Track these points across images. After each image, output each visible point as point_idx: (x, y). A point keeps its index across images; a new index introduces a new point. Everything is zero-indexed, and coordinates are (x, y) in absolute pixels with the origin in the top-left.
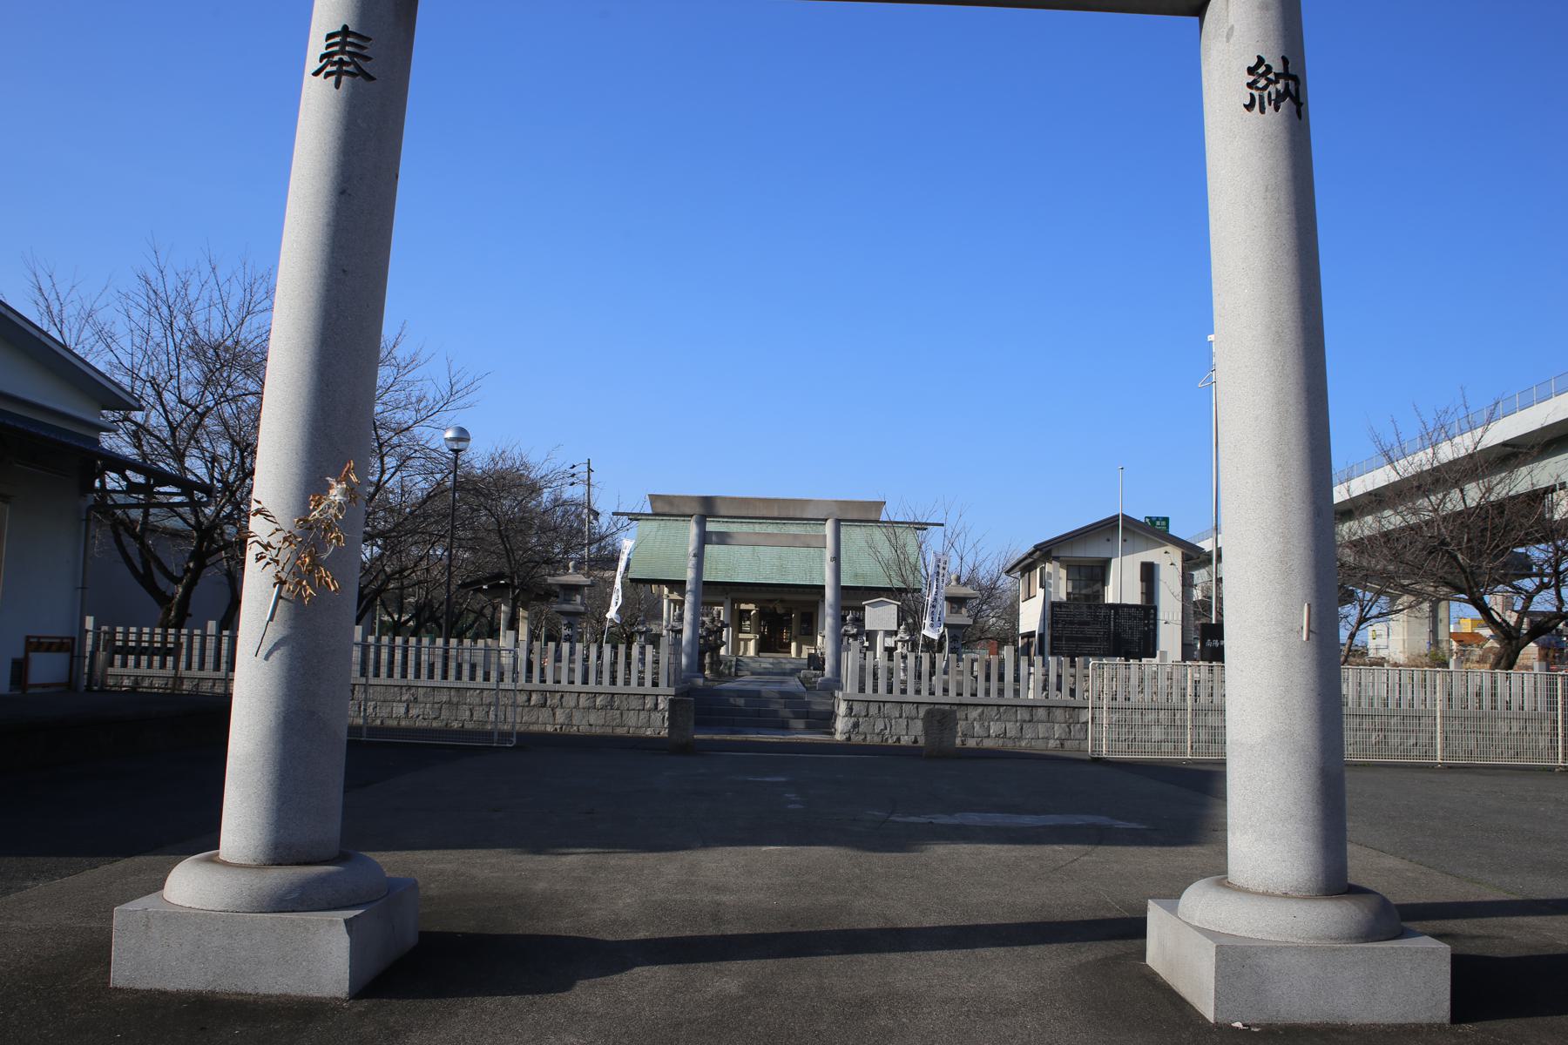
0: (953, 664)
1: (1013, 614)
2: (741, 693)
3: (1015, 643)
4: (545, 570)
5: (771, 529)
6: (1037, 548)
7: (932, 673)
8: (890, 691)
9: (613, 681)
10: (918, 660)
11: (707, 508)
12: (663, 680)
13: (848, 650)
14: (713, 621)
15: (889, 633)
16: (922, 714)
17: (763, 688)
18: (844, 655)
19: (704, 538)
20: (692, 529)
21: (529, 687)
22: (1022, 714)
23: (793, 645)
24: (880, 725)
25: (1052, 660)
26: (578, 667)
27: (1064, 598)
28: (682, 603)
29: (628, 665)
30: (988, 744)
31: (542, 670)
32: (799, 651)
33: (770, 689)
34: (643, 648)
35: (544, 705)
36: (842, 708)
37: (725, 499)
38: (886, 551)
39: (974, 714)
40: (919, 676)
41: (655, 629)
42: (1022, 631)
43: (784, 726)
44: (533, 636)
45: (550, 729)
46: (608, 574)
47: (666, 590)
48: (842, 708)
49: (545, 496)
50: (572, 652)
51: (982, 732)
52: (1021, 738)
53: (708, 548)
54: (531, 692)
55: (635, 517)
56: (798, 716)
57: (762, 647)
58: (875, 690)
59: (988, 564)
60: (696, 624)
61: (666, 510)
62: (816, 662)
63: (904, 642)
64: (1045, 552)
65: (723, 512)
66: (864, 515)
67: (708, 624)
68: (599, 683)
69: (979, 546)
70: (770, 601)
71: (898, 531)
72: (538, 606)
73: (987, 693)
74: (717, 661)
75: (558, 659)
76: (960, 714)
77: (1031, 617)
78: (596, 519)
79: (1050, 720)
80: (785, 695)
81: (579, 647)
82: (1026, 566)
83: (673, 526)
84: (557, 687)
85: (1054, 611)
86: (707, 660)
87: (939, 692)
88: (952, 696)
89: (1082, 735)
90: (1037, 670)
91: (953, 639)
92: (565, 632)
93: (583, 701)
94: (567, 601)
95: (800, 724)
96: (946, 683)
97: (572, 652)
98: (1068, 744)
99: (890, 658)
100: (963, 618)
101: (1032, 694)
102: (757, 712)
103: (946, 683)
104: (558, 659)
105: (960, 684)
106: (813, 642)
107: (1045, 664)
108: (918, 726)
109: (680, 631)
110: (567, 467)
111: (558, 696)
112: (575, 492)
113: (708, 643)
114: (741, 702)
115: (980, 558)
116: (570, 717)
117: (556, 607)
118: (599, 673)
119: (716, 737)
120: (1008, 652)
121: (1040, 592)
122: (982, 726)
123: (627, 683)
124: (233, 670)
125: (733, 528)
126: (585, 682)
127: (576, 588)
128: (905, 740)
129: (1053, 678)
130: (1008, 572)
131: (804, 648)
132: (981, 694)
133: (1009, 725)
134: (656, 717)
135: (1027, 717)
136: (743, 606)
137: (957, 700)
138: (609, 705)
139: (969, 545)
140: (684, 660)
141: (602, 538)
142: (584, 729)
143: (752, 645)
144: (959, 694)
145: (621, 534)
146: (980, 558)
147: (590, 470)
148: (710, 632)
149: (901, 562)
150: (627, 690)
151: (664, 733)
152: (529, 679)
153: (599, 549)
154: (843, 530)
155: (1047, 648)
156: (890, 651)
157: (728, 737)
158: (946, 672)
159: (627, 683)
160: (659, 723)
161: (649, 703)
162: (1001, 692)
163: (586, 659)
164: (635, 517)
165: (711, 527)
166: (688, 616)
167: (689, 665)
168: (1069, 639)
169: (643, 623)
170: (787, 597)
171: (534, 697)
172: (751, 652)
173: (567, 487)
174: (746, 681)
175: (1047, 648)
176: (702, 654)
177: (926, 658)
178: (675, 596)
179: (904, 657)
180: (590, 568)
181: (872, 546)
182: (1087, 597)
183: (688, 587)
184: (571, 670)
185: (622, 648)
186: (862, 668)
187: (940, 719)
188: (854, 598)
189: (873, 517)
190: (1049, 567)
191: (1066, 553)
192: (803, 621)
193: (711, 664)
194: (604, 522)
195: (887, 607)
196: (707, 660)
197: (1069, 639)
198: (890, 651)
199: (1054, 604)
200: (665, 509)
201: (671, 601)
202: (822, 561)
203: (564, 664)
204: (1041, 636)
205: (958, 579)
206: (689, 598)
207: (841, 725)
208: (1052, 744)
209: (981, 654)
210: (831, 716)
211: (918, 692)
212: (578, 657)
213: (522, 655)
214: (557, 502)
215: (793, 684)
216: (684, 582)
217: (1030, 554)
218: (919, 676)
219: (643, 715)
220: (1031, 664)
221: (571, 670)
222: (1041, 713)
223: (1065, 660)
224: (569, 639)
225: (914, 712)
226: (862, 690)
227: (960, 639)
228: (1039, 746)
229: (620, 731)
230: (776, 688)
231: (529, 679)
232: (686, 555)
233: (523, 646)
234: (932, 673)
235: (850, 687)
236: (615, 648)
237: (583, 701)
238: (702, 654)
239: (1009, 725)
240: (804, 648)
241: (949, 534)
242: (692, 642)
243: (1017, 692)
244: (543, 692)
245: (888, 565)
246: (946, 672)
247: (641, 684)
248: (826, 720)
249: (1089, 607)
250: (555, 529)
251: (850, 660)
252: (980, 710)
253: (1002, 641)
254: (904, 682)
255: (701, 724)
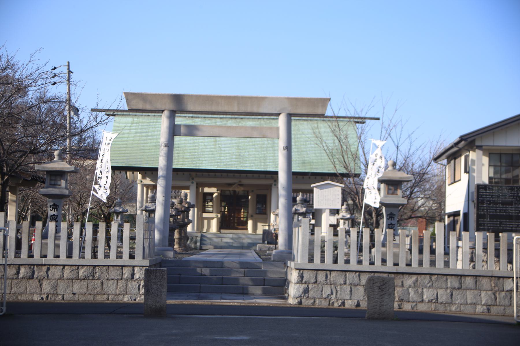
0: (390, 238)
1: (440, 196)
2: (206, 264)
3: (442, 220)
4: (32, 158)
5: (230, 122)
6: (462, 138)
8: (335, 261)
9: (95, 255)
10: (360, 235)
11: (178, 104)
12: (139, 254)
13: (298, 226)
14: (181, 202)
15: (335, 212)
17: (226, 260)
18: (295, 230)
19: (174, 131)
21: (18, 261)
22: (452, 282)
24: (327, 291)
25: (479, 236)
27: (486, 181)
29: (108, 240)
30: (422, 308)
31: (30, 247)
32: (255, 228)
33: (231, 260)
34: (121, 227)
35: (32, 277)
37: (191, 96)
38: (330, 141)
39: (409, 281)
40: (360, 249)
41: (130, 210)
43: (244, 292)
44: (20, 218)
45: (37, 298)
47: (139, 176)
48: (294, 276)
49: (30, 93)
50: (57, 230)
51: (415, 297)
52: (451, 303)
53: (176, 138)
54: (19, 266)
55: (112, 113)
56: (256, 283)
57: (224, 224)
58: (323, 261)
60: (168, 205)
61: (140, 106)
62: (270, 238)
63: (345, 219)
64: (469, 142)
65: (190, 108)
66: (312, 110)
68: (82, 256)
70: (230, 185)
73: (421, 263)
74: (184, 237)
75: (45, 236)
76: (398, 281)
77: (456, 199)
79: (477, 288)
80: (244, 265)
81: (64, 225)
82: (452, 154)
83: (144, 120)
84: (44, 261)
85: (480, 195)
86: (176, 235)
88: (389, 266)
89: (507, 302)
90: (465, 243)
91: (390, 216)
92: (51, 213)
93: (67, 272)
95: (258, 290)
96: (384, 254)
97: (57, 230)
98: (494, 310)
100: (398, 198)
101: (460, 265)
102: (221, 280)
103: (384, 254)
104: (45, 236)
105: (396, 256)
106: (267, 220)
107: (473, 239)
108: (360, 293)
109: (153, 211)
110: (49, 68)
111: (45, 268)
112: (59, 91)
113: (177, 222)
114: (206, 271)
116: (56, 287)
117: (43, 191)
118: (82, 248)
119: (186, 302)
120: (439, 228)
121: (465, 177)
122: (416, 292)
123: (107, 256)
125: (198, 121)
126: (69, 256)
127: (61, 174)
128: (350, 304)
130: (436, 159)
132: (415, 264)
133: (441, 292)
134: (133, 285)
135: (457, 285)
136: (207, 190)
137: (394, 269)
138: (91, 276)
140: (157, 236)
142: (68, 298)
143: (214, 224)
144: (396, 264)
145: (100, 128)
147: (70, 72)
149: (344, 150)
150: (107, 262)
151: (140, 299)
152: (18, 253)
153: (79, 142)
154: (293, 123)
157: (196, 302)
158: (384, 245)
159: (107, 256)
160: (135, 290)
161: (127, 273)
162: (433, 263)
163: (70, 236)
164: (112, 113)
167: (162, 240)
168: (492, 217)
169: (120, 205)
170: (245, 181)
171: (23, 270)
172: (214, 228)
174: (210, 254)
176: (172, 231)
177: (366, 233)
179: (348, 233)
181: (318, 137)
182: (507, 181)
183: (160, 173)
184: (57, 246)
185: (102, 226)
186: (311, 243)
187: (380, 285)
188: (303, 182)
189: (319, 111)
190: (473, 155)
192: (258, 202)
193: (180, 239)
196: (176, 235)
197: (492, 217)
198: (334, 227)
199: (480, 187)
200: (140, 105)
201: (143, 185)
202: (275, 149)
204: (466, 215)
205: (394, 164)
206: (161, 184)
207: (294, 291)
208: (479, 309)
210: (284, 283)
211: (360, 262)
212: (63, 234)
213: (12, 234)
214: (42, 100)
215: (251, 256)
216: (156, 170)
217: (456, 144)
219: (121, 284)
220: (459, 238)
221: (57, 246)
222: (469, 282)
223: (491, 236)
224: (54, 218)
225: (356, 280)
226: (311, 260)
227: (396, 216)
228: (468, 311)
229: (101, 299)
231: (18, 253)
232: (157, 146)
233: (13, 226)
236: (96, 227)
237: (67, 272)
238: (172, 231)
239: (441, 292)
241: (386, 125)
243: (447, 264)
245: (332, 153)
246: (384, 245)
247: (119, 256)
248: (280, 287)
249: (512, 189)
251: (301, 235)
252: (414, 278)
253: (430, 219)
254: (347, 254)
255: (173, 291)
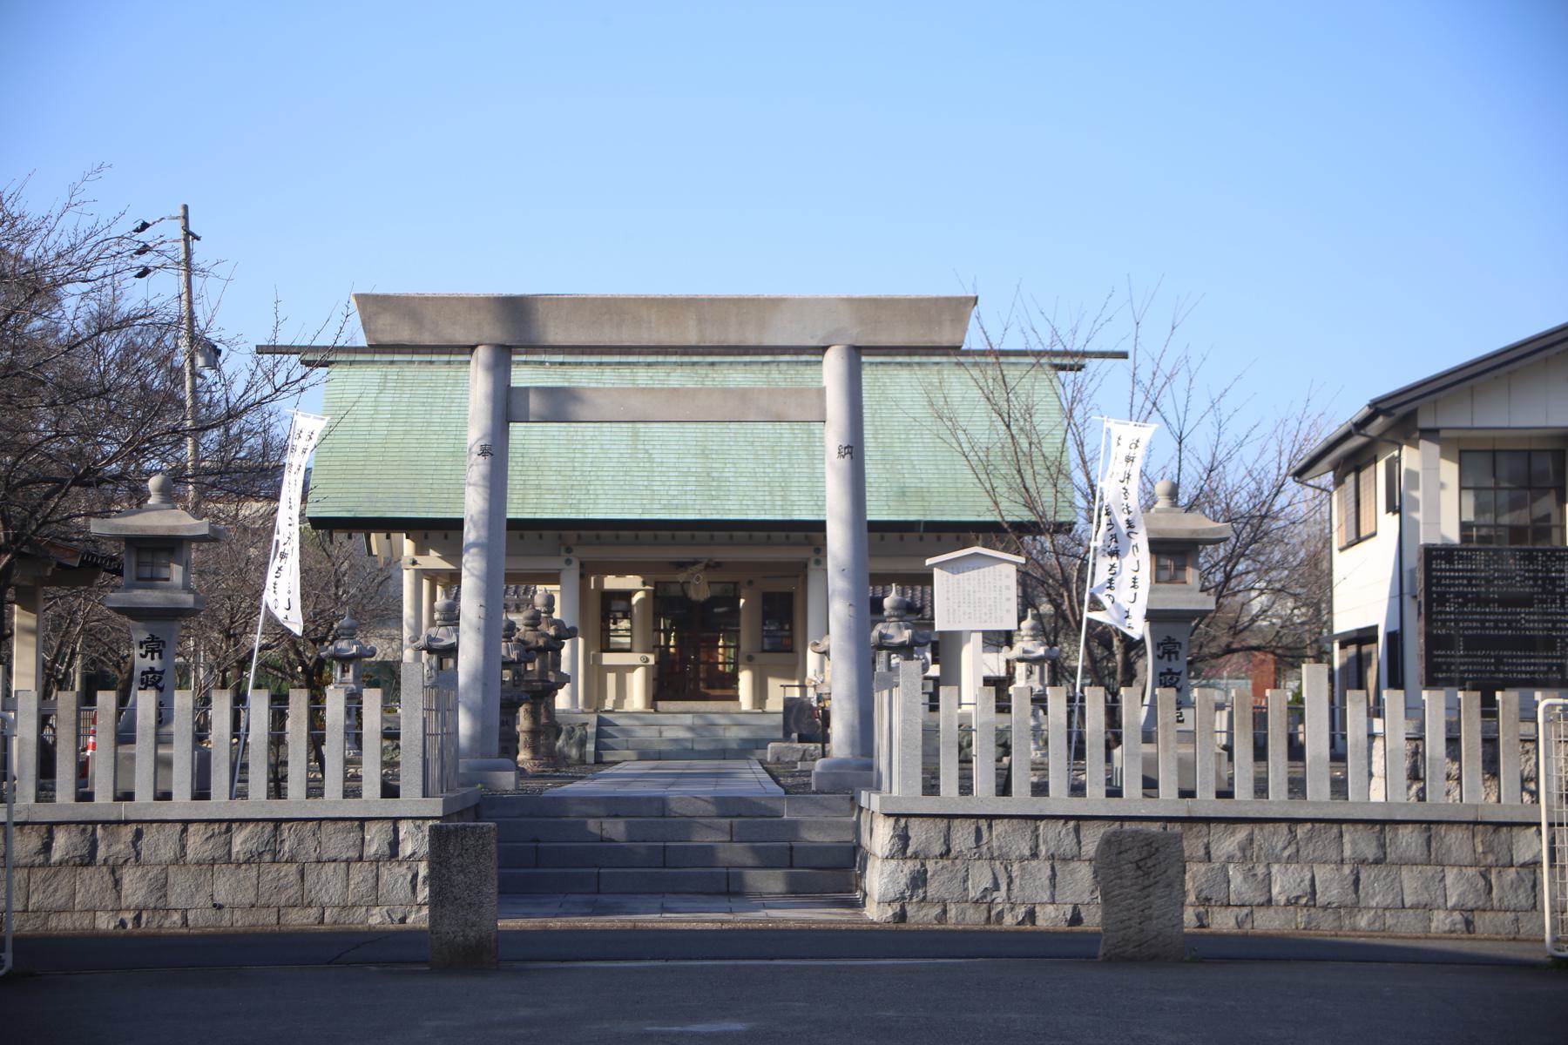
0: (1166, 714)
1: (1315, 584)
2: (614, 806)
3: (1322, 656)
4: (81, 499)
5: (676, 377)
6: (1378, 408)
7: (1114, 738)
8: (1004, 789)
9: (277, 787)
10: (1075, 706)
11: (516, 326)
12: (410, 781)
13: (891, 685)
14: (534, 621)
16: (1090, 846)
17: (674, 792)
18: (880, 698)
19: (508, 407)
20: (474, 384)
21: (45, 813)
22: (1356, 843)
23: (745, 678)
24: (980, 878)
25: (1434, 701)
26: (181, 754)
27: (1453, 535)
28: (453, 579)
29: (316, 740)
30: (1268, 922)
32: (760, 693)
33: (690, 792)
34: (354, 700)
35: (89, 860)
36: (880, 838)
37: (556, 301)
38: (981, 427)
39: (1228, 843)
40: (1078, 750)
41: (383, 651)
42: (1337, 630)
43: (730, 889)
44: (51, 680)
45: (105, 923)
46: (252, 509)
47: (408, 546)
48: (880, 838)
49: (70, 304)
50: (163, 716)
51: (1247, 891)
52: (1355, 907)
53: (516, 429)
54: (51, 826)
55: (319, 357)
56: (767, 864)
57: (665, 686)
58: (966, 788)
59: (1249, 454)
60: (495, 629)
61: (405, 335)
62: (806, 721)
64: (1399, 417)
65: (555, 336)
66: (918, 334)
67: (523, 631)
69: (1226, 406)
70: (681, 565)
71: (1012, 374)
72: (61, 598)
73: (1261, 788)
74: (548, 728)
75: (125, 735)
76: (1193, 845)
77: (1364, 590)
78: (213, 364)
79: (1432, 858)
80: (729, 807)
81: (183, 701)
82: (1349, 456)
84: (124, 810)
85: (1433, 577)
86: (523, 722)
87: (1132, 788)
88: (1167, 800)
89: (1523, 899)
90: (1394, 725)
91: (1166, 649)
92: (143, 662)
93: (196, 842)
94: (150, 581)
95: (772, 881)
96: (1150, 763)
97: (163, 716)
98: (1484, 922)
99: (1003, 707)
100: (1189, 595)
101: (1379, 788)
102: (662, 856)
103: (1150, 763)
104: (125, 735)
105: (1186, 767)
106: (794, 669)
107: (1414, 711)
108: (1080, 883)
109: (452, 651)
110: (127, 226)
111: (127, 833)
112: (159, 292)
113: (524, 681)
114: (616, 829)
115: (1228, 438)
116: (162, 887)
117: (117, 598)
118: (239, 769)
119: (556, 923)
120: (1312, 680)
121: (1388, 525)
122: (1250, 875)
124: (1301, 720)
125: (582, 377)
126: (201, 791)
127: (170, 546)
128: (1050, 917)
129: (1435, 744)
130: (1299, 474)
131: (774, 684)
132: (1243, 790)
133: (1323, 873)
134: (395, 878)
135: (1371, 852)
136: (612, 583)
137: (1182, 808)
138: (267, 853)
139: (1200, 404)
140: (465, 725)
141: (233, 414)
142: (201, 919)
143: (637, 684)
144: (1187, 794)
145: (284, 404)
146: (1228, 438)
147: (189, 236)
148: (528, 651)
150: (316, 809)
151: (419, 918)
152: (45, 790)
153: (227, 443)
154: (867, 375)
155: (1414, 664)
156: (999, 685)
157: (587, 923)
158: (1148, 737)
159: (315, 790)
161: (376, 839)
162: (1297, 786)
163: (201, 732)
164: (319, 357)
165: (521, 376)
166: (470, 607)
167: (479, 738)
168: (1473, 643)
169: (350, 634)
171: (61, 840)
173: (128, 281)
174: (626, 776)
175: (1414, 664)
176: (509, 708)
177: (1095, 699)
178: (433, 560)
179: (1039, 701)
180: (202, 495)
182: (1517, 533)
183: (470, 534)
185: (299, 701)
186: (930, 733)
187: (1141, 856)
188: (902, 551)
189: (945, 338)
190: (1410, 458)
191: (1455, 418)
192: (767, 616)
193: (534, 733)
194: (238, 366)
195: (989, 572)
196: (523, 722)
197: (1473, 643)
198: (999, 685)
199: (1433, 554)
200: (402, 333)
201: (421, 574)
202: (814, 455)
203: (143, 749)
204: (1395, 640)
205: (1173, 493)
206: (472, 568)
207: (880, 881)
208: (1440, 921)
209: (1234, 687)
211: (1077, 789)
212: (182, 726)
214: (105, 324)
215: (750, 779)
216: (457, 525)
217: (1360, 426)
218: (1078, 750)
219: (359, 873)
220: (1376, 710)
222: (1408, 840)
223: (1469, 701)
224: (153, 680)
225: (1069, 844)
226: (931, 787)
228: (1405, 928)
229: (298, 919)
230: (706, 789)
232: (458, 455)
234: (1114, 738)
235: (899, 779)
237: (196, 842)
238: (509, 708)
239: (1323, 873)
240: (774, 684)
241: (1144, 376)
242: (484, 676)
243: (1339, 787)
244: (86, 825)
245: (987, 466)
246: (1148, 737)
247: (352, 790)
248: (839, 870)
249: (1529, 557)
250: (104, 392)
251: (898, 710)
252: (1242, 832)
253: (1286, 656)
254: (1040, 767)
255: (515, 891)
